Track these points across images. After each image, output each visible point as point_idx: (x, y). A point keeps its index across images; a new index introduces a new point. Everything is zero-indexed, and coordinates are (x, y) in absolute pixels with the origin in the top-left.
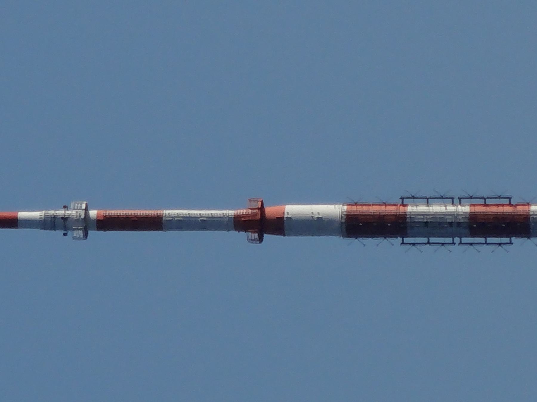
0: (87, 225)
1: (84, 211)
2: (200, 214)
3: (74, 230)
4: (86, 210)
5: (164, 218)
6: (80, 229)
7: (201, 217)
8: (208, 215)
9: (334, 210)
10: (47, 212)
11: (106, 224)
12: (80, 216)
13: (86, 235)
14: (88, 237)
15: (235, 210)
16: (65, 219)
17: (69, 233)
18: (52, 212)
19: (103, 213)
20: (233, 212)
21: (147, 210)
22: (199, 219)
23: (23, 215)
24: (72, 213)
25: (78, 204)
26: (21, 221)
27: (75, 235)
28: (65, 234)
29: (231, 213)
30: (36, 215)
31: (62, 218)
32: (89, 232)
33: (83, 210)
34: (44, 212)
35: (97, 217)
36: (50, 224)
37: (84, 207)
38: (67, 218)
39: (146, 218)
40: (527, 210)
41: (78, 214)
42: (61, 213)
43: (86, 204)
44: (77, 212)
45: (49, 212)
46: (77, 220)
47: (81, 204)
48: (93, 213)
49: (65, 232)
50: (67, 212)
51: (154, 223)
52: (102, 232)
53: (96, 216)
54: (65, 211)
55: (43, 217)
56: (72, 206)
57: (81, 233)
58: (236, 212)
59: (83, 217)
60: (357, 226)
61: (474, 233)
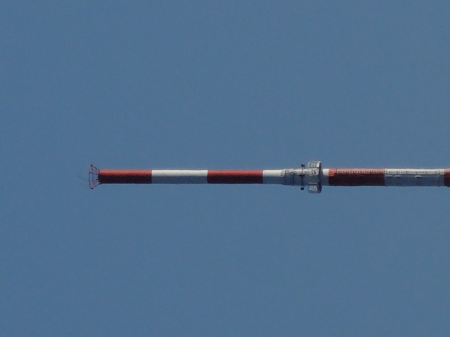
0: (320, 181)
1: (318, 169)
2: (407, 172)
3: (310, 185)
4: (320, 168)
5: (386, 176)
6: (315, 184)
7: (417, 175)
8: (423, 172)
9: (205, 172)
10: (287, 170)
11: (337, 180)
12: (315, 173)
13: (320, 189)
14: (322, 191)
15: (445, 169)
16: (302, 176)
17: (306, 187)
18: (291, 170)
19: (334, 171)
20: (444, 170)
21: (349, 168)
22: (416, 176)
23: (267, 172)
24: (307, 171)
25: (313, 163)
26: (264, 177)
27: (310, 189)
28: (302, 189)
29: (442, 171)
30: (278, 172)
31: (300, 175)
32: (323, 187)
33: (318, 168)
34: (284, 170)
35: (329, 175)
36: (290, 180)
37: (318, 165)
38: (304, 175)
39: (366, 174)
40: (261, 173)
41: (313, 172)
42: (299, 171)
43: (320, 163)
44: (312, 170)
45: (290, 170)
46: (313, 177)
47: (316, 163)
48: (326, 171)
49: (302, 187)
50: (304, 170)
51: (377, 180)
52: (334, 187)
53: (328, 173)
54: (303, 169)
55: (284, 174)
56: (309, 166)
57: (315, 188)
58: (446, 170)
59: (317, 174)
60: (212, 179)
61: (209, 182)
